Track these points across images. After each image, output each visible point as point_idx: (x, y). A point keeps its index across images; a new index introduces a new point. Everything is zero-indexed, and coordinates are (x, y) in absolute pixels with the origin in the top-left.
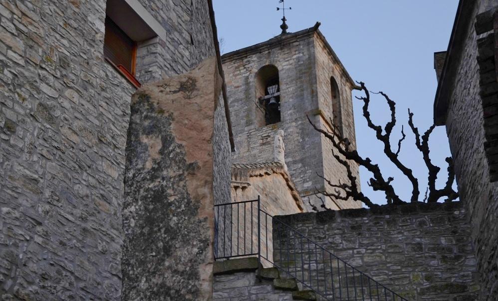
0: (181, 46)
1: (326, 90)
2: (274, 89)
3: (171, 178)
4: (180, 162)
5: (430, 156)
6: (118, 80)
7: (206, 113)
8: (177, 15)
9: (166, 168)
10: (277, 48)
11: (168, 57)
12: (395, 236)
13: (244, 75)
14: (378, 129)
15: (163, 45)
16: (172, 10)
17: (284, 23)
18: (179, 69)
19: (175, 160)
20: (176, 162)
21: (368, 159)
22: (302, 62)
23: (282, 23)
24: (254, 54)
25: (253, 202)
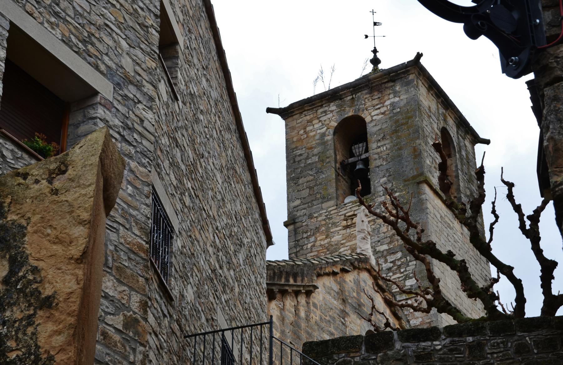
0: (140, 106)
2: (361, 149)
3: (15, 322)
4: (32, 295)
6: (23, 161)
7: (79, 216)
8: (133, 60)
9: (10, 305)
10: (364, 92)
11: (117, 122)
13: (319, 131)
15: (108, 106)
16: (124, 55)
17: (375, 56)
18: (135, 139)
19: (24, 292)
20: (26, 296)
21: (450, 252)
22: (399, 110)
23: (372, 56)
24: (332, 102)
25: (235, 330)
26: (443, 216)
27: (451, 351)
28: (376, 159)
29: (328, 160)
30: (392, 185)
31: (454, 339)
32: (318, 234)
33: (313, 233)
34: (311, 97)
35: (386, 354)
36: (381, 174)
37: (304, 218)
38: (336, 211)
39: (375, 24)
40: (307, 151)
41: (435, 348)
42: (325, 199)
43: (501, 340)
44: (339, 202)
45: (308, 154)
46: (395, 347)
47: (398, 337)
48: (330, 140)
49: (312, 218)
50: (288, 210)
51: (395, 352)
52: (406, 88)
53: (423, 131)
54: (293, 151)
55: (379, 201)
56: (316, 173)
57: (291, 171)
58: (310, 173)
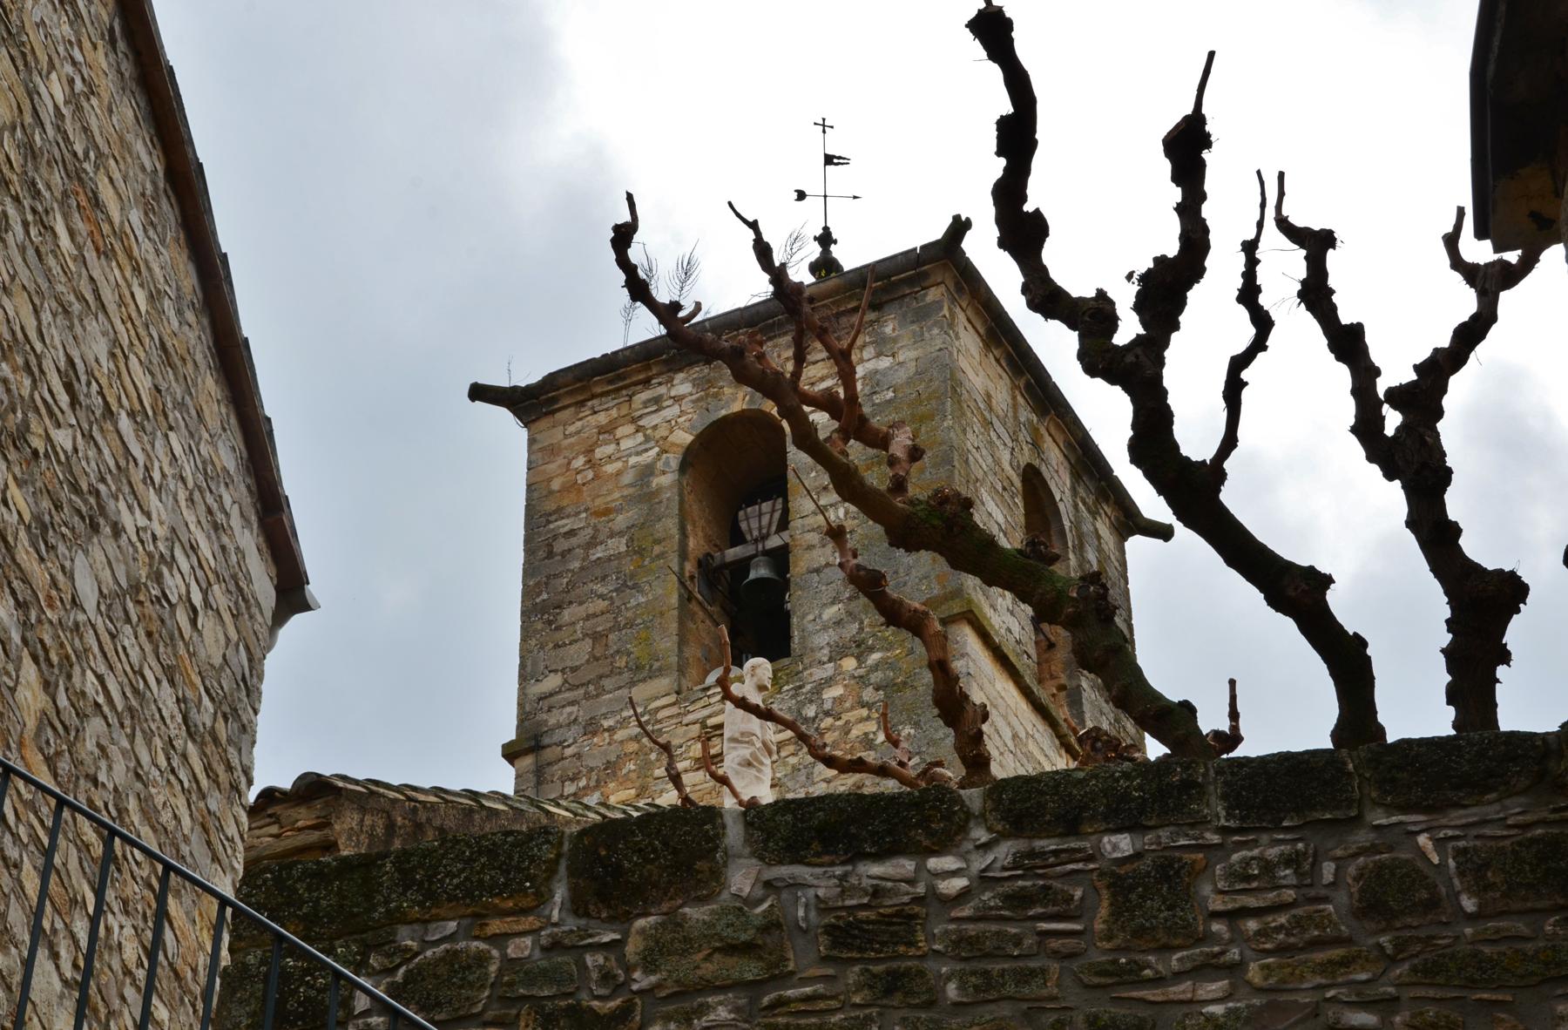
1: (1001, 520)
5: (1456, 503)
12: (1181, 990)
14: (1090, 318)
22: (891, 394)
24: (680, 370)
26: (1022, 735)
27: (1020, 900)
28: (810, 547)
29: (657, 549)
30: (861, 629)
31: (1039, 844)
32: (611, 785)
33: (598, 781)
34: (615, 353)
35: (674, 922)
36: (827, 592)
37: (570, 735)
38: (674, 710)
39: (829, 160)
40: (593, 521)
41: (932, 889)
42: (641, 671)
43: (1286, 848)
44: (685, 684)
45: (596, 530)
46: (724, 885)
47: (748, 840)
48: (670, 487)
49: (594, 734)
50: (520, 705)
51: (725, 911)
52: (915, 327)
53: (967, 461)
54: (549, 522)
55: (816, 677)
56: (616, 590)
57: (538, 584)
58: (601, 589)
